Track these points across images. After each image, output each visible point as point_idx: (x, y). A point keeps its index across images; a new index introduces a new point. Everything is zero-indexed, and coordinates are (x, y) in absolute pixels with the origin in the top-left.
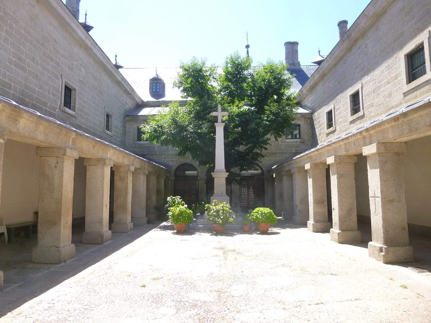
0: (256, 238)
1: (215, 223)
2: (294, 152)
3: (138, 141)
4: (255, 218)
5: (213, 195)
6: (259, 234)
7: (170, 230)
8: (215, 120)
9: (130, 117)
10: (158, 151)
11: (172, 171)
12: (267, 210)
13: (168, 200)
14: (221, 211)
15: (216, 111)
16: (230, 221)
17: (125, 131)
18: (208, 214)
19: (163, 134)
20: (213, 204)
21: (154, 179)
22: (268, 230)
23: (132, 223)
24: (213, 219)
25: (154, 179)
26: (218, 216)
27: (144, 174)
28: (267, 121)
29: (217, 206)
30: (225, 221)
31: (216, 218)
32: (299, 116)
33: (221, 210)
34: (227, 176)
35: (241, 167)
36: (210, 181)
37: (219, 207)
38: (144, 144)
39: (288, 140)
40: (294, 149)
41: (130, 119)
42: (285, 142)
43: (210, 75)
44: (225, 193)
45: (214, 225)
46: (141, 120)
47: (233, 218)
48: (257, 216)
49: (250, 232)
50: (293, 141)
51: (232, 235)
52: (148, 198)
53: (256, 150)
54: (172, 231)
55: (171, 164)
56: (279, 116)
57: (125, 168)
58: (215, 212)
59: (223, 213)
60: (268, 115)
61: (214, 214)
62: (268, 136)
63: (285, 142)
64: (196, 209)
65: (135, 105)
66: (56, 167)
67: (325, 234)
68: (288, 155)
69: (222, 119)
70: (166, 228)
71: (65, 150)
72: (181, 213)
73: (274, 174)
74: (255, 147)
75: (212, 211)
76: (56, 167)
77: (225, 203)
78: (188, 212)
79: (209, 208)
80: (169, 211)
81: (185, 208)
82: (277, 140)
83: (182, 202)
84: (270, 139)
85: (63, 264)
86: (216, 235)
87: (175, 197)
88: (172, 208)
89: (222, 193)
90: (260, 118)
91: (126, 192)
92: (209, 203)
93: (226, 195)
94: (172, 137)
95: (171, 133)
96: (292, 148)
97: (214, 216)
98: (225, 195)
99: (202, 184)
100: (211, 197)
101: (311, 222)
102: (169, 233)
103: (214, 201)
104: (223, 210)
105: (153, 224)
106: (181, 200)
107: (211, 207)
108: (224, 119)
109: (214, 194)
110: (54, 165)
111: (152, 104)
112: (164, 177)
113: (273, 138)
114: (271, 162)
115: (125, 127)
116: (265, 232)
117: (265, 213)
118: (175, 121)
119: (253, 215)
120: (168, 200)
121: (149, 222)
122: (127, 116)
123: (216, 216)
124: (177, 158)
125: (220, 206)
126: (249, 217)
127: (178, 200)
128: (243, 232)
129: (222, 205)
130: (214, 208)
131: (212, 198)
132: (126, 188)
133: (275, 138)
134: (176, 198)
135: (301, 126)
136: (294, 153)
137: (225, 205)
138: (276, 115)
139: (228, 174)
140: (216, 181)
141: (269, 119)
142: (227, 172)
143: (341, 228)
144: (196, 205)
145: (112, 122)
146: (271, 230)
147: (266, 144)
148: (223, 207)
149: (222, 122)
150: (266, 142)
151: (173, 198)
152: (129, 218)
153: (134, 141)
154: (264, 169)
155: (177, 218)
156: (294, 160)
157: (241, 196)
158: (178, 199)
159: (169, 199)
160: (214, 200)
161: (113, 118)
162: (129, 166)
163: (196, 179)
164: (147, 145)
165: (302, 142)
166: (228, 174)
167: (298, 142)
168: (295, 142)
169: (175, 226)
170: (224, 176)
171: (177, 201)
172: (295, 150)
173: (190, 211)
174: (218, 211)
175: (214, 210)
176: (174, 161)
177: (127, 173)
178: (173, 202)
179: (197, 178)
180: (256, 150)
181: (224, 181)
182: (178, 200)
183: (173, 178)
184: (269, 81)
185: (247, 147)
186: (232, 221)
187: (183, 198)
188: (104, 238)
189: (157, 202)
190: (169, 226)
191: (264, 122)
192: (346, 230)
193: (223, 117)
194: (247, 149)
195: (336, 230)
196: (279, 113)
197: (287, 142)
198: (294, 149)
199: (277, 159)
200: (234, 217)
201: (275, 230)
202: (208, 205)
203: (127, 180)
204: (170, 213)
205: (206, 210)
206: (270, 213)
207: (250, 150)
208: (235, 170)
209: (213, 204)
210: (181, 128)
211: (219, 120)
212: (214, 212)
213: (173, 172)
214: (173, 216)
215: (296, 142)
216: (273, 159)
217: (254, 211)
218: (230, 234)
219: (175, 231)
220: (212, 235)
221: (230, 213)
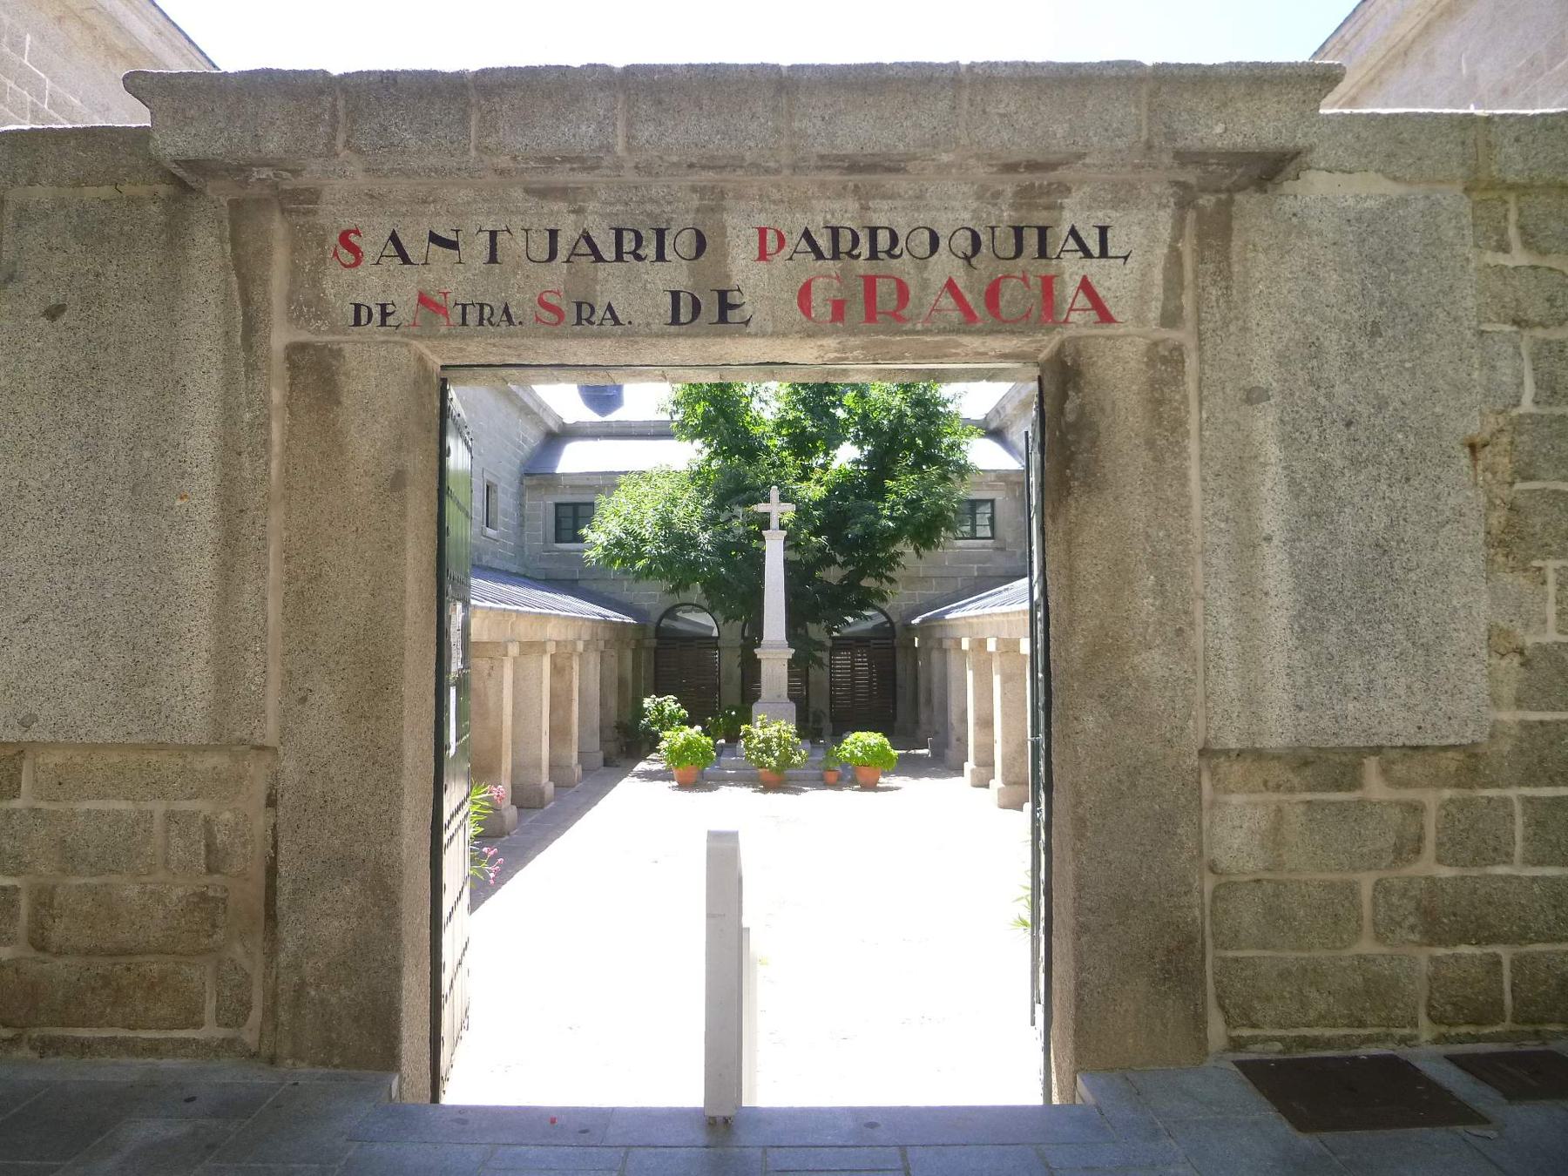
0: (849, 798)
1: (762, 765)
2: (976, 574)
3: (557, 541)
6: (856, 790)
7: (664, 779)
8: (764, 521)
9: (535, 477)
12: (874, 739)
15: (767, 501)
17: (522, 516)
18: (746, 746)
19: (640, 556)
20: (758, 724)
22: (877, 782)
23: (580, 766)
24: (758, 757)
26: (768, 751)
27: (596, 650)
28: (891, 518)
30: (785, 761)
32: (992, 477)
35: (871, 459)
36: (751, 669)
37: (771, 731)
39: (960, 543)
41: (535, 482)
43: (752, 395)
44: (786, 695)
45: (760, 770)
46: (565, 486)
47: (800, 754)
48: (852, 753)
49: (838, 784)
51: (797, 791)
52: (603, 704)
53: (867, 582)
54: (667, 784)
55: (645, 604)
56: (920, 508)
57: (566, 647)
58: (763, 741)
59: (779, 745)
60: (895, 504)
62: (899, 547)
65: (542, 437)
66: (489, 675)
67: (600, 803)
69: (780, 519)
70: (650, 776)
71: (506, 647)
72: (689, 745)
73: (916, 639)
74: (861, 573)
75: (756, 741)
76: (489, 675)
77: (783, 722)
78: (703, 741)
79: (748, 733)
80: (662, 739)
82: (920, 556)
84: (902, 554)
85: (507, 837)
86: (765, 790)
88: (667, 734)
89: (779, 696)
90: (875, 511)
91: (570, 701)
92: (749, 722)
94: (662, 564)
95: (660, 554)
97: (760, 750)
99: (729, 663)
100: (752, 704)
101: (969, 766)
102: (662, 787)
104: (780, 738)
105: (617, 766)
106: (679, 705)
107: (753, 730)
108: (785, 520)
110: (487, 672)
111: (589, 430)
113: (910, 551)
114: (915, 601)
115: (522, 505)
116: (870, 786)
117: (869, 745)
118: (666, 523)
119: (845, 749)
120: (645, 706)
121: (607, 762)
122: (527, 474)
123: (765, 752)
125: (772, 729)
126: (837, 753)
128: (822, 782)
129: (778, 727)
130: (760, 732)
131: (755, 707)
132: (570, 690)
133: (917, 551)
135: (997, 504)
136: (976, 578)
137: (785, 728)
138: (913, 504)
139: (793, 651)
140: (765, 667)
142: (790, 646)
143: (1007, 782)
145: (497, 500)
146: (884, 781)
147: (892, 569)
148: (779, 731)
149: (782, 527)
150: (893, 558)
151: (657, 699)
152: (575, 754)
153: (545, 541)
155: (678, 755)
156: (948, 620)
158: (670, 704)
159: (647, 703)
160: (759, 716)
161: (499, 490)
162: (574, 643)
165: (997, 549)
166: (793, 651)
169: (675, 772)
172: (979, 568)
173: (708, 739)
174: (767, 741)
175: (759, 737)
177: (570, 658)
178: (658, 710)
180: (867, 582)
181: (783, 670)
183: (653, 643)
184: (901, 415)
185: (846, 572)
187: (683, 701)
188: (546, 796)
189: (619, 716)
190: (659, 771)
191: (884, 522)
192: (1015, 783)
193: (783, 514)
194: (845, 578)
195: (997, 783)
196: (919, 499)
197: (960, 548)
200: (803, 752)
201: (895, 781)
203: (571, 674)
204: (663, 745)
205: (744, 736)
206: (882, 746)
207: (851, 583)
208: (816, 631)
209: (758, 724)
210: (683, 542)
211: (774, 524)
212: (760, 743)
213: (652, 627)
214: (671, 750)
215: (984, 547)
217: (848, 740)
218: (792, 789)
219: (675, 783)
220: (755, 792)
221: (793, 744)
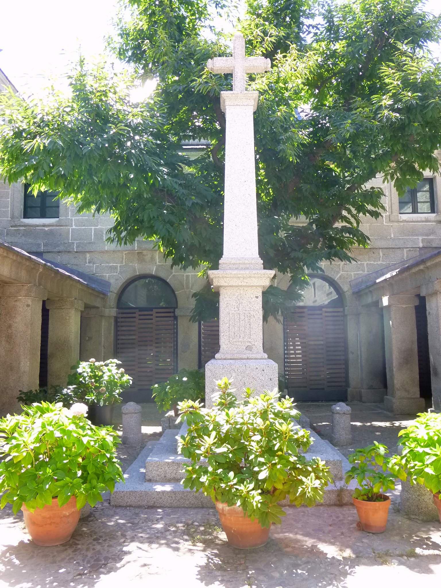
2: (421, 245)
4: (430, 471)
5: (217, 356)
10: (75, 242)
11: (109, 294)
13: (79, 370)
14: (258, 437)
16: (303, 494)
21: (28, 306)
25: (28, 306)
28: (392, 108)
29: (232, 411)
31: (231, 474)
33: (260, 431)
34: (267, 283)
38: (38, 226)
39: (404, 217)
40: (420, 238)
42: (398, 222)
50: (419, 220)
61: (222, 454)
63: (398, 222)
64: (163, 400)
68: (405, 253)
81: (75, 419)
83: (122, 375)
87: (102, 363)
89: (249, 348)
93: (266, 356)
96: (417, 235)
98: (259, 356)
103: (219, 382)
107: (203, 411)
109: (218, 351)
112: (80, 306)
114: (364, 271)
120: (79, 370)
124: (122, 262)
127: (110, 371)
130: (221, 418)
134: (107, 365)
141: (399, 106)
144: (163, 388)
148: (264, 415)
151: (97, 364)
153: (13, 217)
154: (345, 288)
157: (287, 358)
163: (172, 314)
164: (46, 229)
167: (430, 221)
168: (423, 221)
170: (256, 282)
171: (109, 374)
175: (217, 426)
176: (116, 267)
179: (174, 312)
182: (110, 371)
186: (315, 489)
198: (420, 238)
199: (379, 263)
202: (191, 403)
213: (112, 297)
216: (369, 263)
